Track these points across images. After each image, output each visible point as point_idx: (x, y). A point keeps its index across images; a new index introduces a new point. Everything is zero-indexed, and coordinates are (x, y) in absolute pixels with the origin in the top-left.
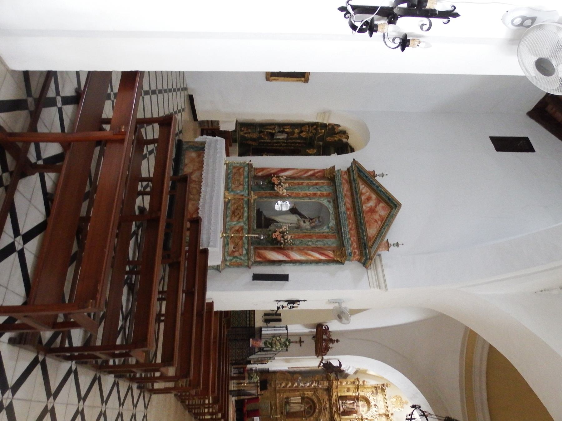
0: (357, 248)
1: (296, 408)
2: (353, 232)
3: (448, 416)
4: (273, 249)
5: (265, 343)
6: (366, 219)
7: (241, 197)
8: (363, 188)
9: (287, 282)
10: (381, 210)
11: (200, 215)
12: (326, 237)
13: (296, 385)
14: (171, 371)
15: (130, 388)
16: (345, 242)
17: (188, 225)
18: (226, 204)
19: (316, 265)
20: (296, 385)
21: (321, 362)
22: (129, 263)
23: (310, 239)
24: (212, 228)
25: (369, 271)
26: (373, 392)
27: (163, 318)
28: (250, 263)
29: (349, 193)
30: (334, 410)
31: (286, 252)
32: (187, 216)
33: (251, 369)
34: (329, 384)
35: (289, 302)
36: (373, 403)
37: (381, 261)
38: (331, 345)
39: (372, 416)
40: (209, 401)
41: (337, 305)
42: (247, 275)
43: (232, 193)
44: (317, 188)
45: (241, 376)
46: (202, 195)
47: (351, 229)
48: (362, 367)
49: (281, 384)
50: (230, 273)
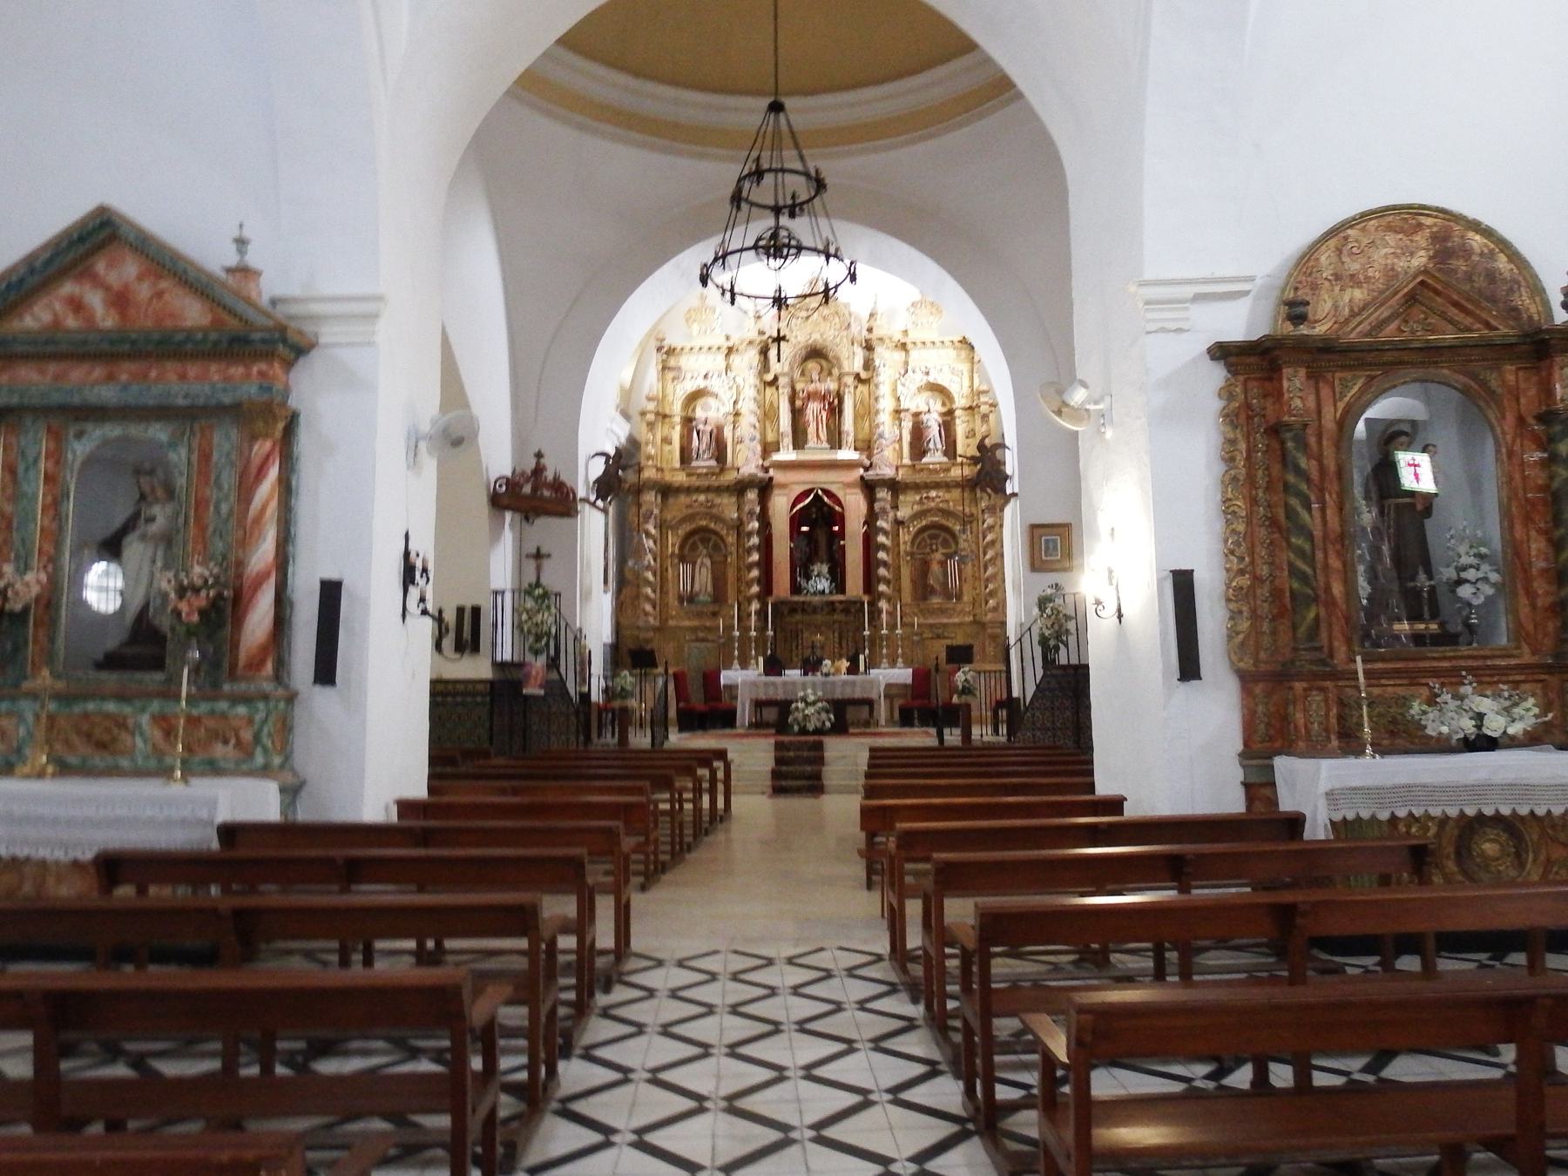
0: (246, 366)
1: (704, 579)
2: (193, 370)
3: (728, 200)
4: (238, 621)
5: (536, 653)
6: (149, 323)
7: (44, 720)
8: (36, 318)
9: (1195, 573)
10: (125, 270)
11: (88, 855)
12: (206, 457)
13: (650, 576)
14: (558, 907)
15: (606, 1013)
16: (227, 399)
17: (125, 891)
18: (64, 769)
19: (297, 494)
20: (650, 576)
21: (593, 504)
22: (230, 1067)
23: (212, 508)
24: (149, 813)
25: (322, 340)
26: (674, 379)
27: (430, 944)
28: (280, 691)
29: (52, 368)
30: (714, 481)
31: (247, 583)
32: (95, 899)
33: (606, 691)
34: (652, 488)
35: (408, 580)
36: (701, 383)
37: (295, 300)
38: (549, 475)
39: (731, 388)
40: (664, 801)
41: (423, 445)
42: (319, 703)
43: (27, 751)
44: (27, 470)
45: (623, 719)
46: (22, 852)
47: (183, 377)
48: (612, 398)
49: (646, 614)
50: (308, 754)
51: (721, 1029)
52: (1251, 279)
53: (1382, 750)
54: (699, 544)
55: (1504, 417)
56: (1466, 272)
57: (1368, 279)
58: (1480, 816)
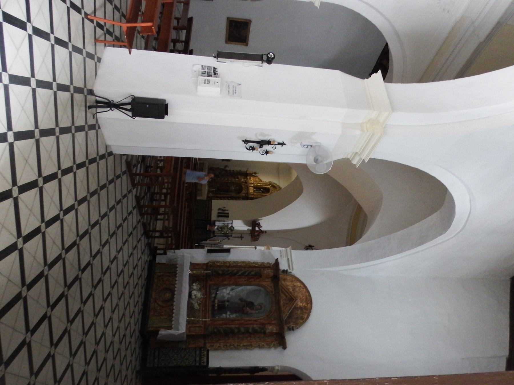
53: (190, 275)
56: (297, 313)
57: (295, 292)
58: (175, 294)
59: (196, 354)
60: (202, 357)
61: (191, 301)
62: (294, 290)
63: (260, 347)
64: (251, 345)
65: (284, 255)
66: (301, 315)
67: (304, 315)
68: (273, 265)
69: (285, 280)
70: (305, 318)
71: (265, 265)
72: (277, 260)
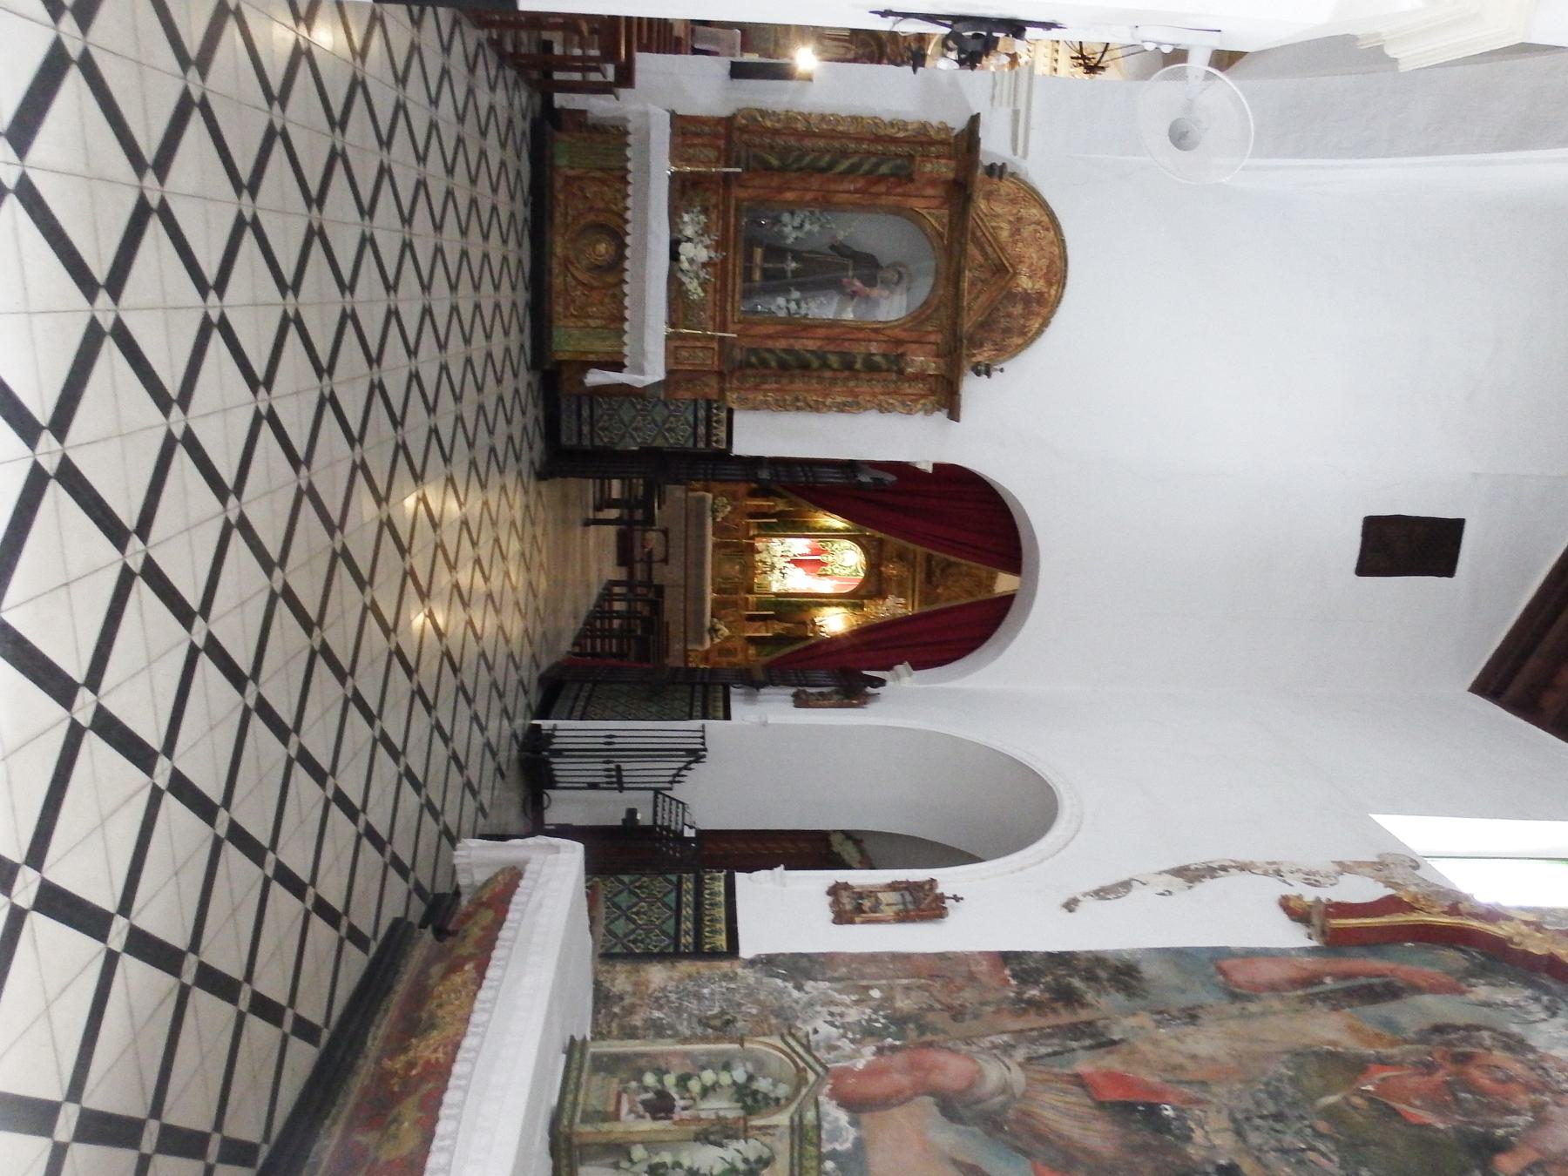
51: (370, 301)
52: (1025, 156)
53: (673, 178)
54: (867, 50)
55: (905, 330)
57: (1015, 242)
58: (626, 246)
59: (696, 417)
60: (716, 428)
61: (680, 275)
62: (1016, 232)
63: (883, 409)
64: (858, 404)
65: (1005, 92)
66: (1022, 321)
67: (1032, 322)
68: (956, 136)
69: (989, 196)
70: (1034, 330)
71: (932, 133)
72: (975, 120)
